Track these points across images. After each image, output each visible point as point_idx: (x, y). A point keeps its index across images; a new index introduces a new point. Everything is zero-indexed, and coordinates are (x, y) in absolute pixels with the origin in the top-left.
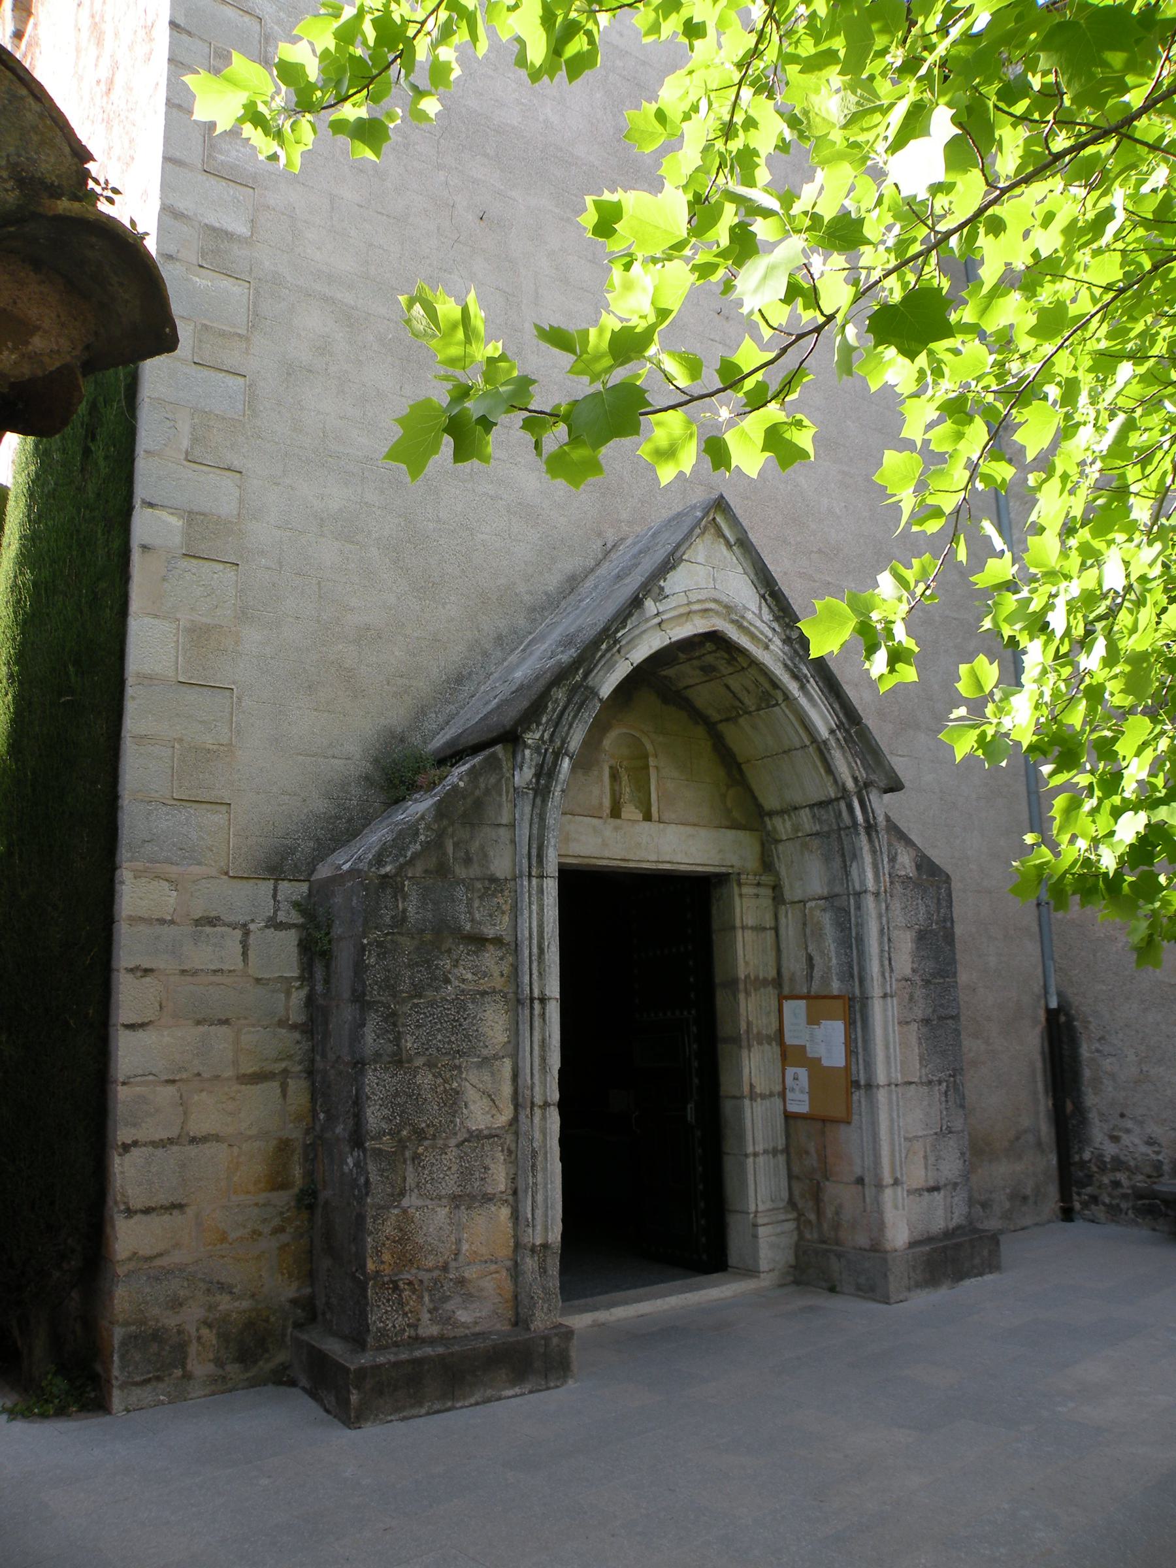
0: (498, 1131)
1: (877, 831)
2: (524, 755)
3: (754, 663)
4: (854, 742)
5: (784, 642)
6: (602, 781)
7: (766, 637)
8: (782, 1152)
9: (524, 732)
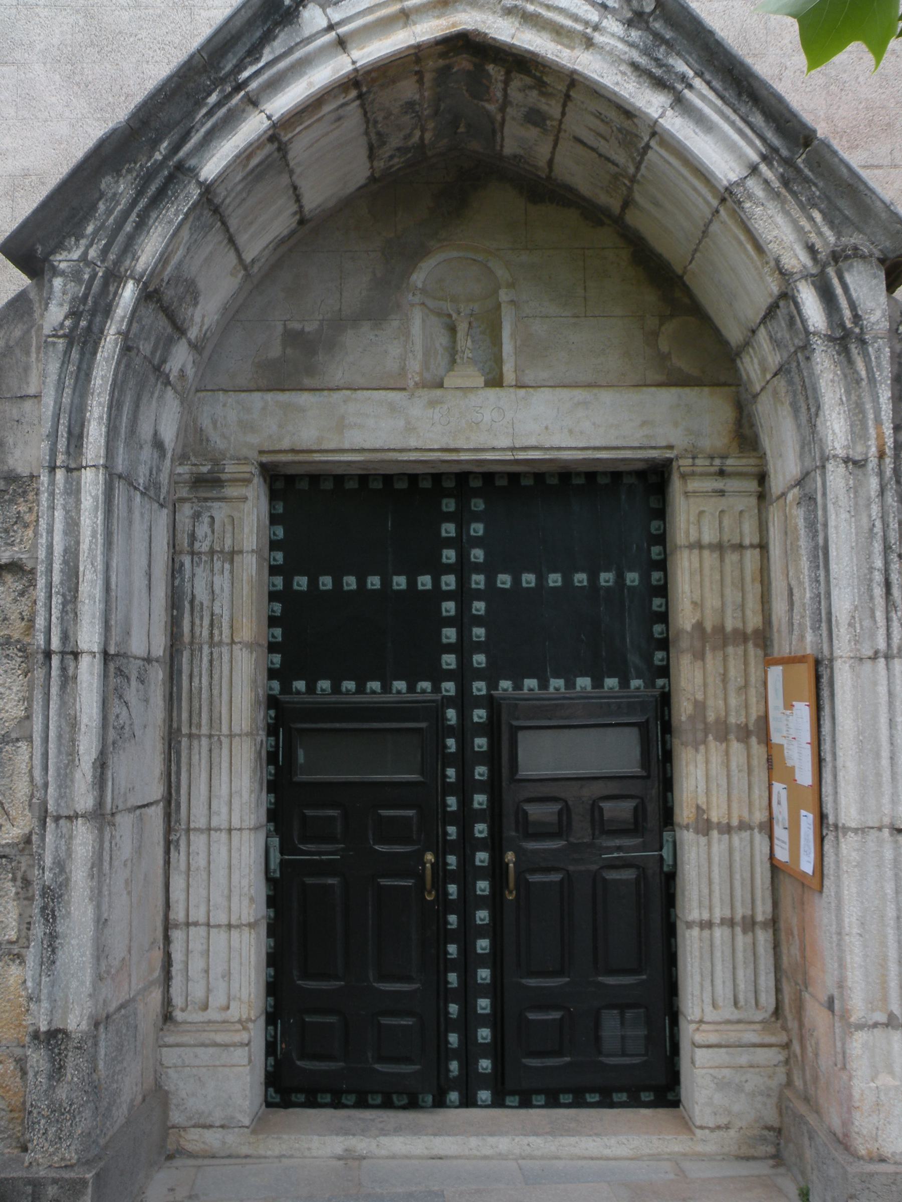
0: (7, 851)
1: (863, 342)
2: (51, 287)
3: (573, 81)
4: (806, 180)
5: (630, 23)
6: (408, 334)
7: (587, 23)
8: (765, 925)
9: (53, 252)
